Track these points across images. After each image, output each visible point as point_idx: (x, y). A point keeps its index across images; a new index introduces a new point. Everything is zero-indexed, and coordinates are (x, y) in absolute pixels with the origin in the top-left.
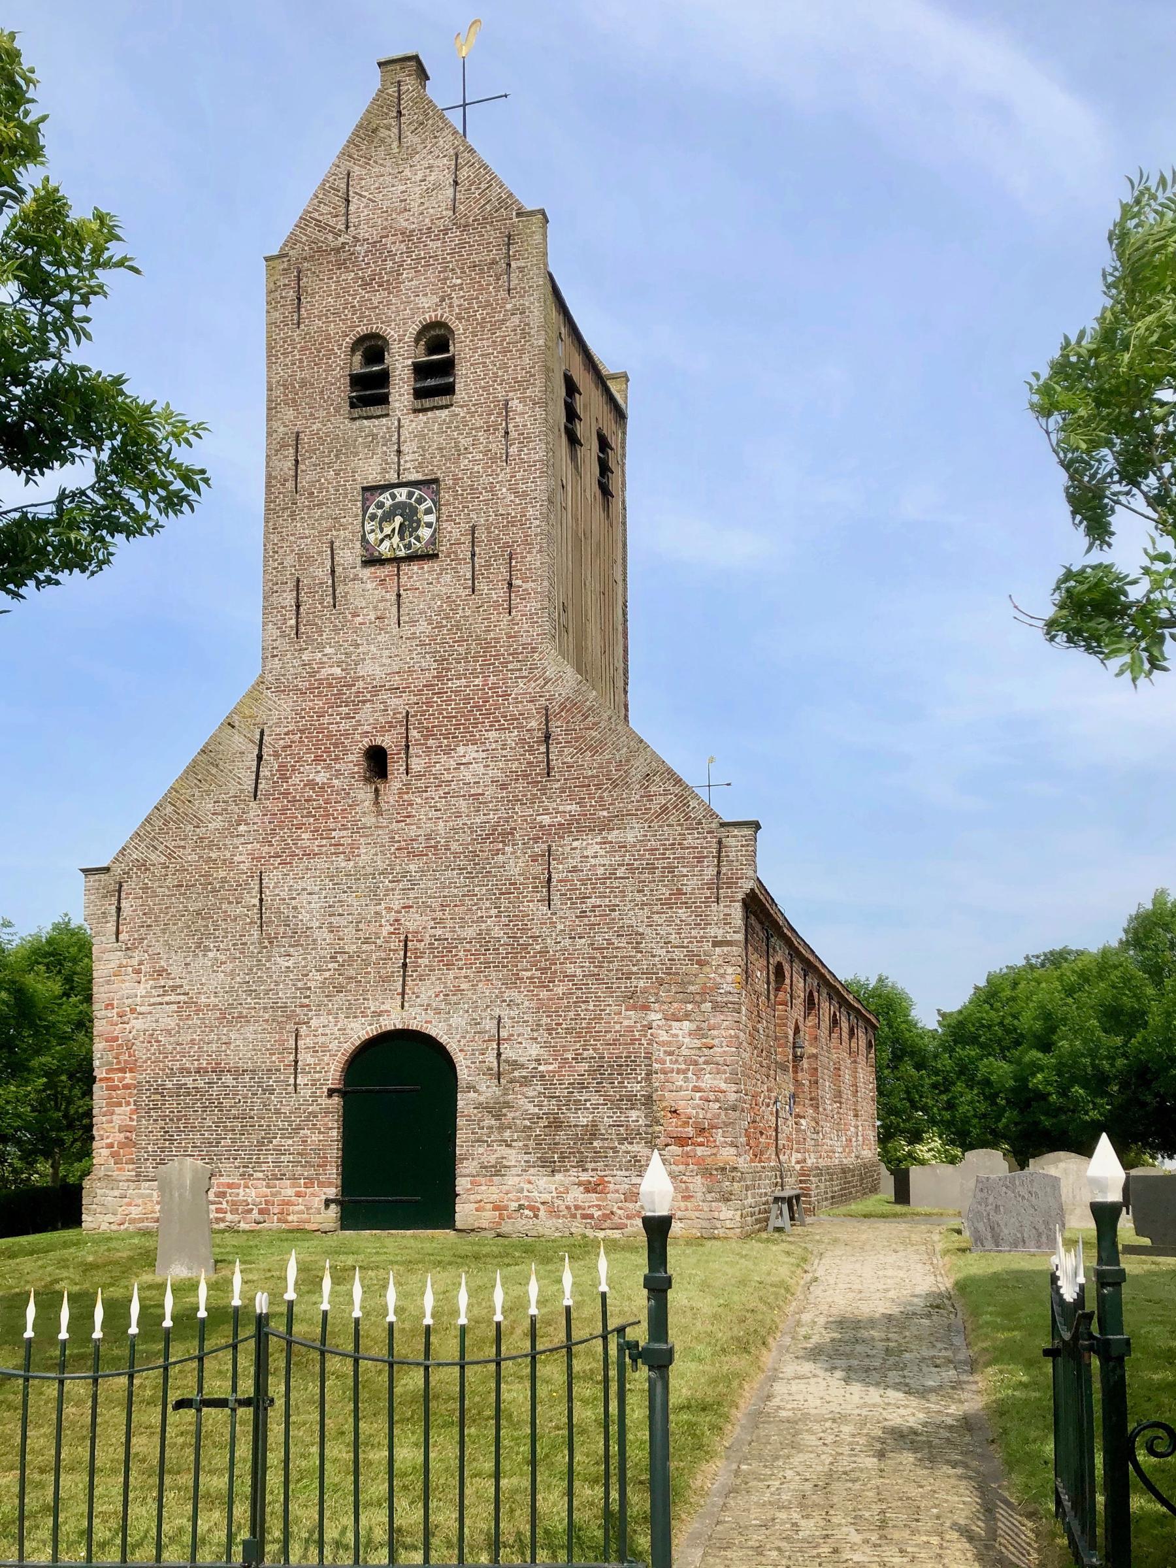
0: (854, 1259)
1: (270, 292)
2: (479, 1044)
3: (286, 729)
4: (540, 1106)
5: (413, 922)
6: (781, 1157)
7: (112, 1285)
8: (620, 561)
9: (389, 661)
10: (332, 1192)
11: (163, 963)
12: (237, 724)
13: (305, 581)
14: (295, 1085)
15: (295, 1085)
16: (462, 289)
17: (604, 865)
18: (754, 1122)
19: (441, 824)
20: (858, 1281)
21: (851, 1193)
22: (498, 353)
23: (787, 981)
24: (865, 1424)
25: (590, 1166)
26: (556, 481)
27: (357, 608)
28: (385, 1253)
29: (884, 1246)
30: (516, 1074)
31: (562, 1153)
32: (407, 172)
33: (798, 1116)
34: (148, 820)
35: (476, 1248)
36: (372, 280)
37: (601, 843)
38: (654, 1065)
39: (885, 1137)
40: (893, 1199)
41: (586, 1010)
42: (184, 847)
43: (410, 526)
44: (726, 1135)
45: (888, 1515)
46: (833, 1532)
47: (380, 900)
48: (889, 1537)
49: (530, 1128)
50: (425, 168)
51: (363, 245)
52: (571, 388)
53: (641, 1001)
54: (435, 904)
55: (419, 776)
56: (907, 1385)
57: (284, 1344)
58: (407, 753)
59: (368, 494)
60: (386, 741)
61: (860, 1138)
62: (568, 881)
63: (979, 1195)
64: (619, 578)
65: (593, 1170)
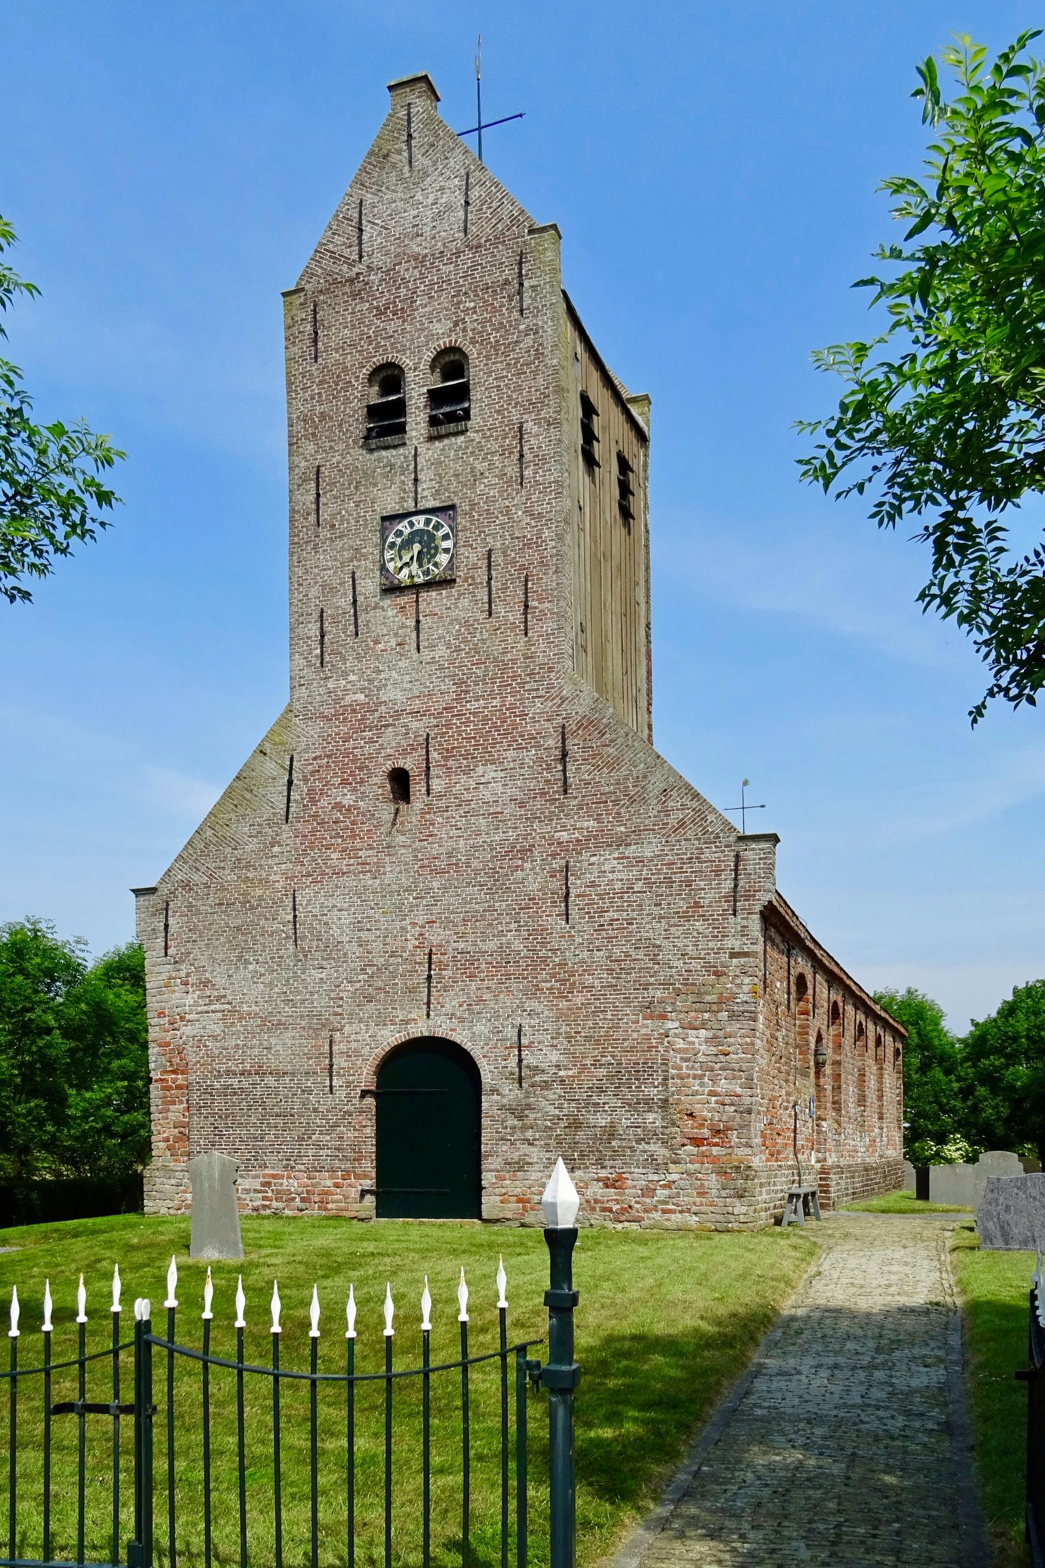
0: (861, 1253)
1: (288, 327)
2: (500, 1051)
3: (314, 755)
4: (560, 1108)
5: (436, 936)
6: (799, 1156)
7: (148, 1266)
8: (642, 583)
9: (409, 685)
10: (369, 1183)
11: (207, 975)
12: (268, 751)
13: (329, 612)
14: (331, 1087)
15: (331, 1087)
16: (475, 312)
17: (622, 880)
18: (771, 1124)
19: (462, 842)
20: (861, 1276)
21: (873, 1189)
22: (513, 375)
23: (810, 991)
24: (840, 1426)
25: (608, 1163)
26: (572, 502)
27: (378, 636)
28: (408, 1241)
29: (894, 1242)
30: (537, 1078)
31: (581, 1151)
32: (419, 196)
33: (819, 1118)
34: (190, 843)
35: (493, 1238)
36: (386, 309)
37: (618, 858)
38: (671, 1071)
39: (912, 1137)
40: (915, 1196)
41: (604, 1019)
42: (223, 868)
43: (428, 552)
44: (741, 1136)
45: (844, 1529)
46: (782, 1546)
47: (406, 915)
48: (840, 1555)
49: (550, 1128)
50: (437, 191)
51: (376, 274)
52: (588, 409)
53: (659, 1010)
54: (457, 918)
55: (440, 797)
56: (892, 1385)
57: (165, 1352)
58: (428, 775)
59: (387, 523)
60: (407, 764)
61: (885, 1139)
62: (587, 895)
63: (990, 1196)
64: (642, 600)
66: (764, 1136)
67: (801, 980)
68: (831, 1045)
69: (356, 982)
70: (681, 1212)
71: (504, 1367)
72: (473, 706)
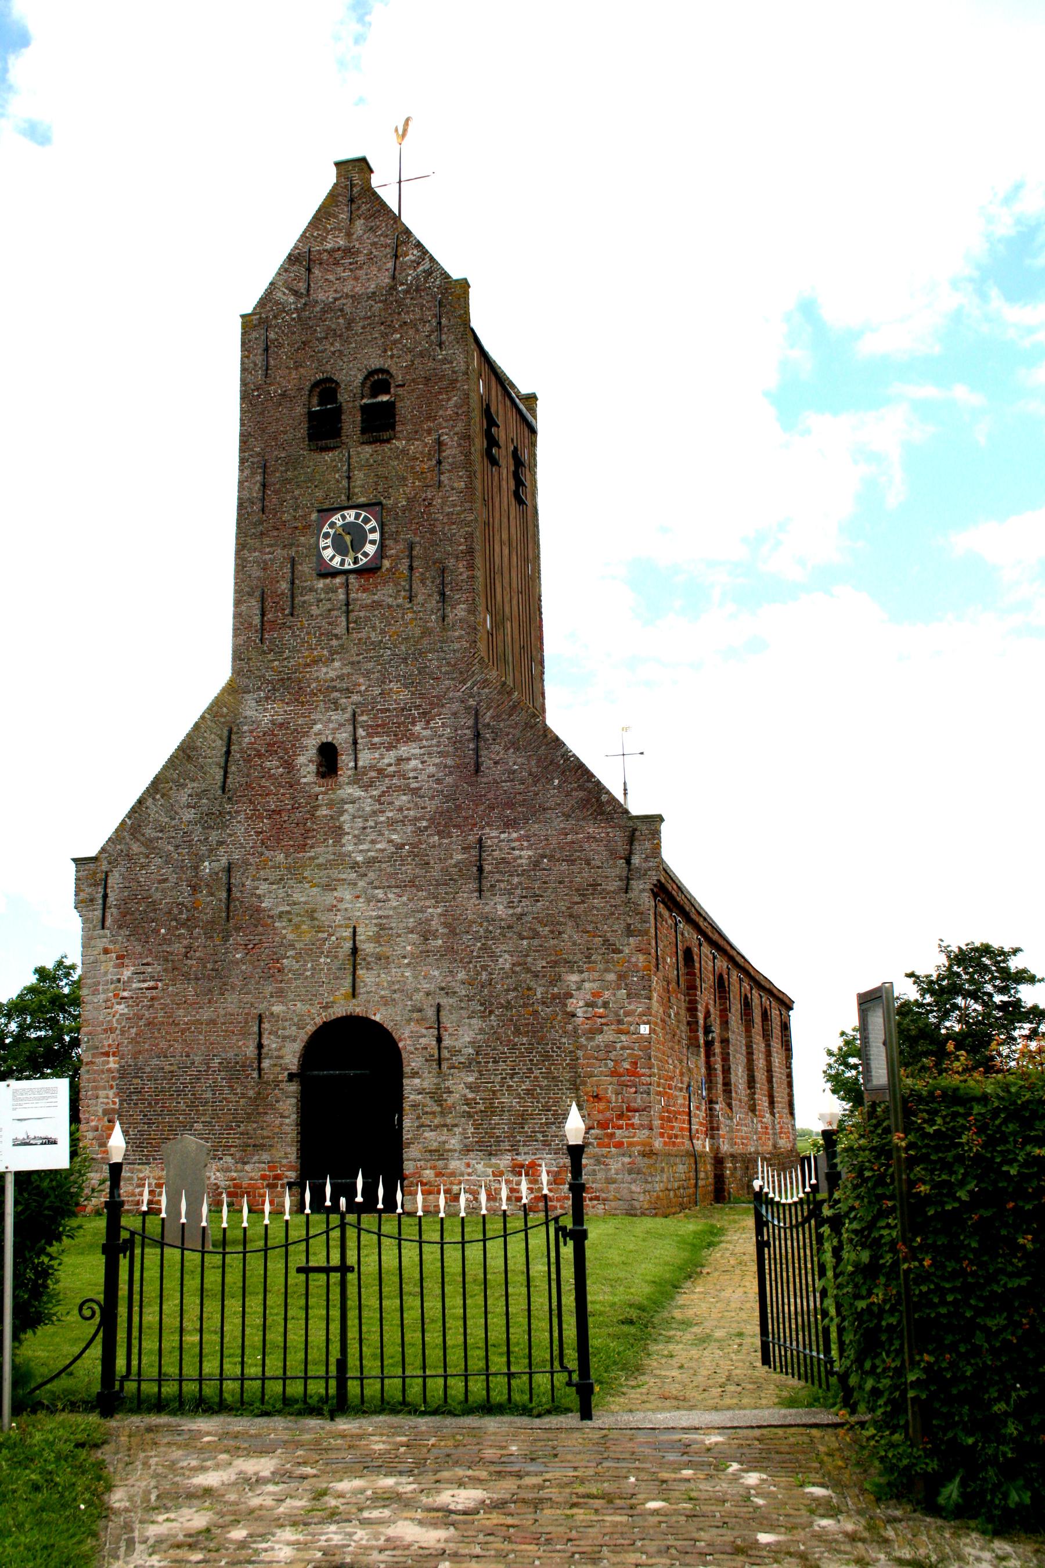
23: (697, 965)
65: (525, 1154)
67: (688, 953)
68: (718, 1021)
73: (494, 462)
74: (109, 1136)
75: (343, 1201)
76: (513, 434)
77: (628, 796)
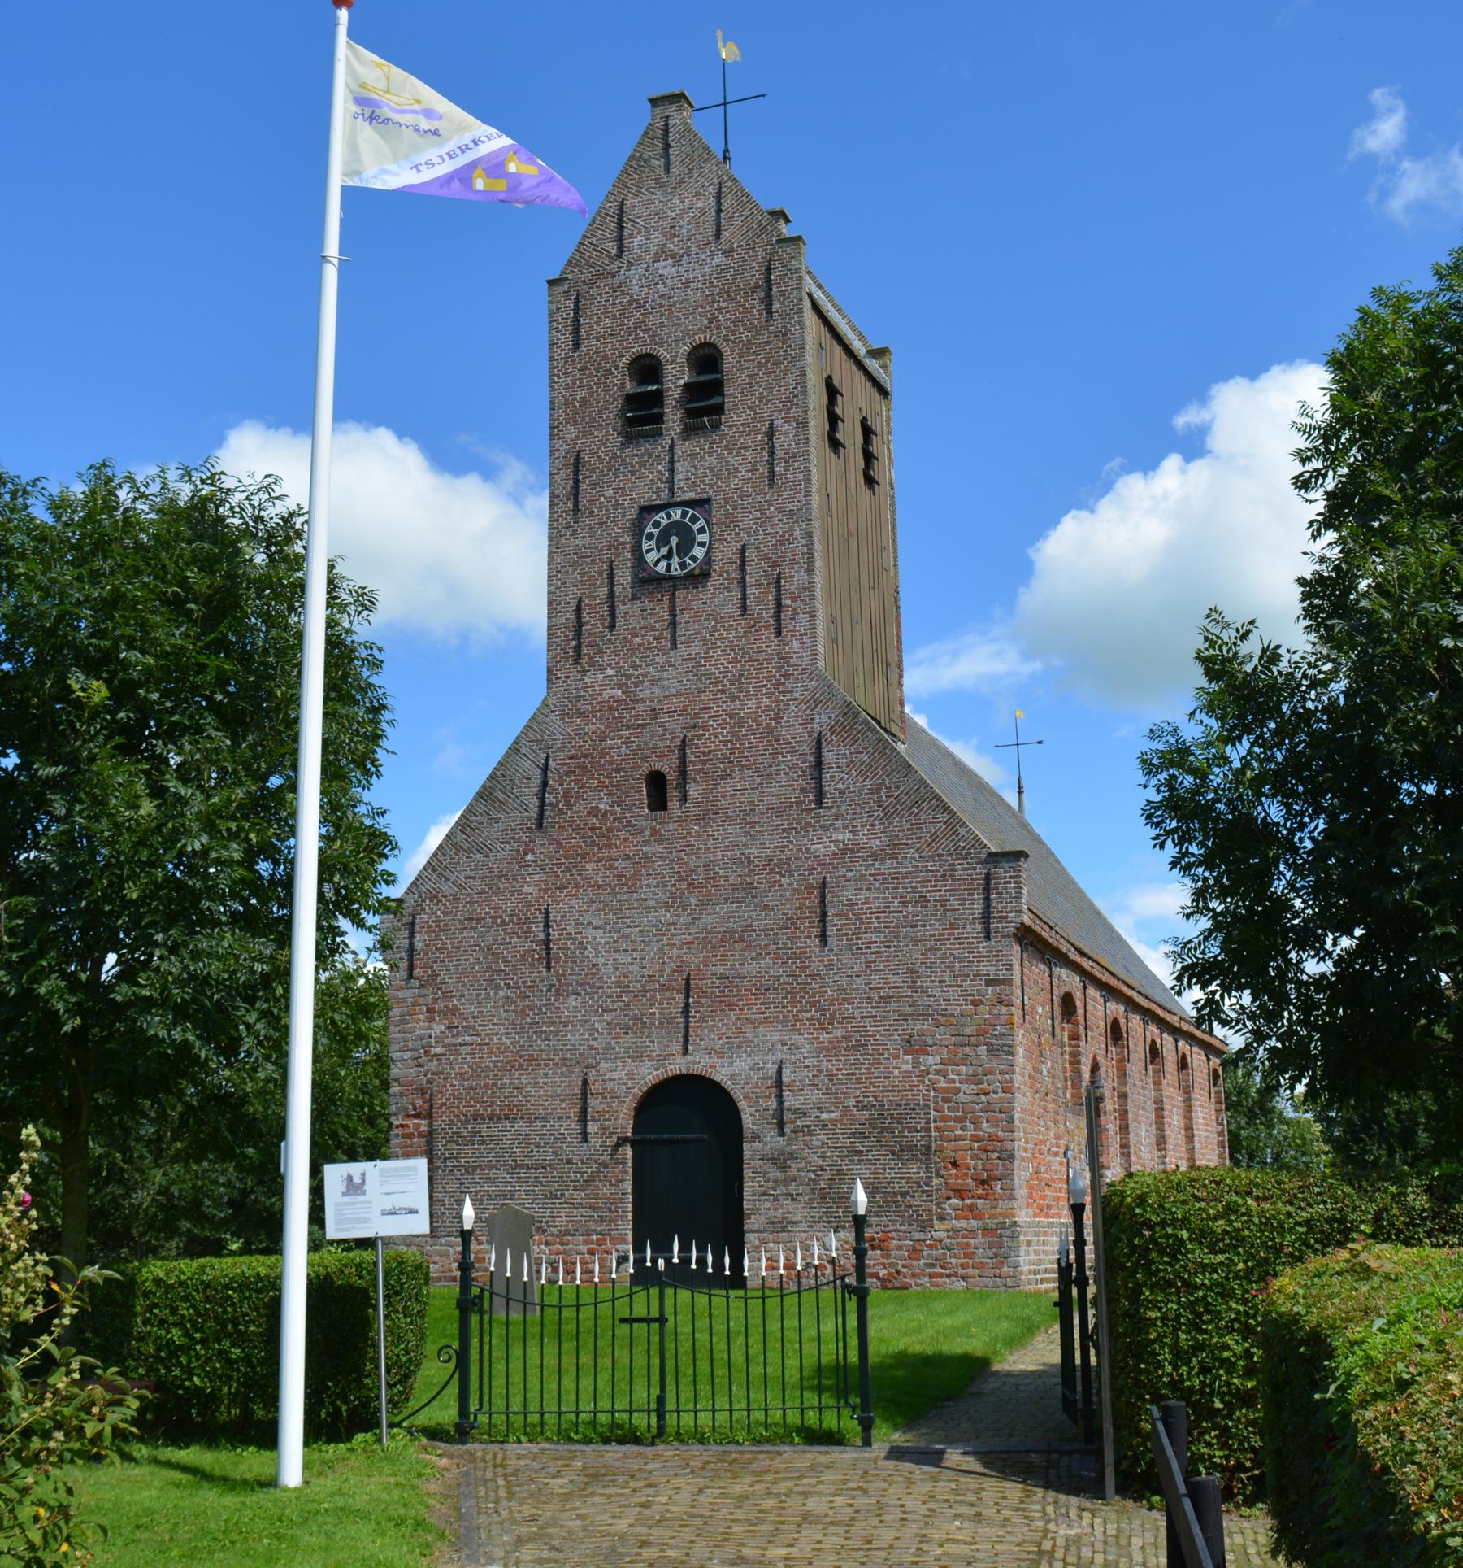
4: (823, 1157)
23: (1080, 1011)
42: (474, 878)
49: (814, 1180)
55: (696, 803)
59: (645, 515)
60: (668, 767)
66: (1030, 1187)
67: (1068, 1002)
69: (611, 1011)
70: (948, 1276)
71: (835, 1288)
72: (730, 707)
73: (835, 444)
74: (462, 1210)
75: (661, 1262)
76: (860, 402)
77: (1024, 796)
